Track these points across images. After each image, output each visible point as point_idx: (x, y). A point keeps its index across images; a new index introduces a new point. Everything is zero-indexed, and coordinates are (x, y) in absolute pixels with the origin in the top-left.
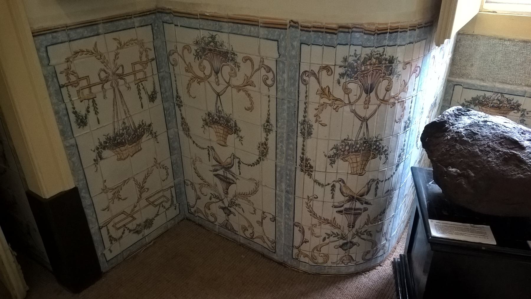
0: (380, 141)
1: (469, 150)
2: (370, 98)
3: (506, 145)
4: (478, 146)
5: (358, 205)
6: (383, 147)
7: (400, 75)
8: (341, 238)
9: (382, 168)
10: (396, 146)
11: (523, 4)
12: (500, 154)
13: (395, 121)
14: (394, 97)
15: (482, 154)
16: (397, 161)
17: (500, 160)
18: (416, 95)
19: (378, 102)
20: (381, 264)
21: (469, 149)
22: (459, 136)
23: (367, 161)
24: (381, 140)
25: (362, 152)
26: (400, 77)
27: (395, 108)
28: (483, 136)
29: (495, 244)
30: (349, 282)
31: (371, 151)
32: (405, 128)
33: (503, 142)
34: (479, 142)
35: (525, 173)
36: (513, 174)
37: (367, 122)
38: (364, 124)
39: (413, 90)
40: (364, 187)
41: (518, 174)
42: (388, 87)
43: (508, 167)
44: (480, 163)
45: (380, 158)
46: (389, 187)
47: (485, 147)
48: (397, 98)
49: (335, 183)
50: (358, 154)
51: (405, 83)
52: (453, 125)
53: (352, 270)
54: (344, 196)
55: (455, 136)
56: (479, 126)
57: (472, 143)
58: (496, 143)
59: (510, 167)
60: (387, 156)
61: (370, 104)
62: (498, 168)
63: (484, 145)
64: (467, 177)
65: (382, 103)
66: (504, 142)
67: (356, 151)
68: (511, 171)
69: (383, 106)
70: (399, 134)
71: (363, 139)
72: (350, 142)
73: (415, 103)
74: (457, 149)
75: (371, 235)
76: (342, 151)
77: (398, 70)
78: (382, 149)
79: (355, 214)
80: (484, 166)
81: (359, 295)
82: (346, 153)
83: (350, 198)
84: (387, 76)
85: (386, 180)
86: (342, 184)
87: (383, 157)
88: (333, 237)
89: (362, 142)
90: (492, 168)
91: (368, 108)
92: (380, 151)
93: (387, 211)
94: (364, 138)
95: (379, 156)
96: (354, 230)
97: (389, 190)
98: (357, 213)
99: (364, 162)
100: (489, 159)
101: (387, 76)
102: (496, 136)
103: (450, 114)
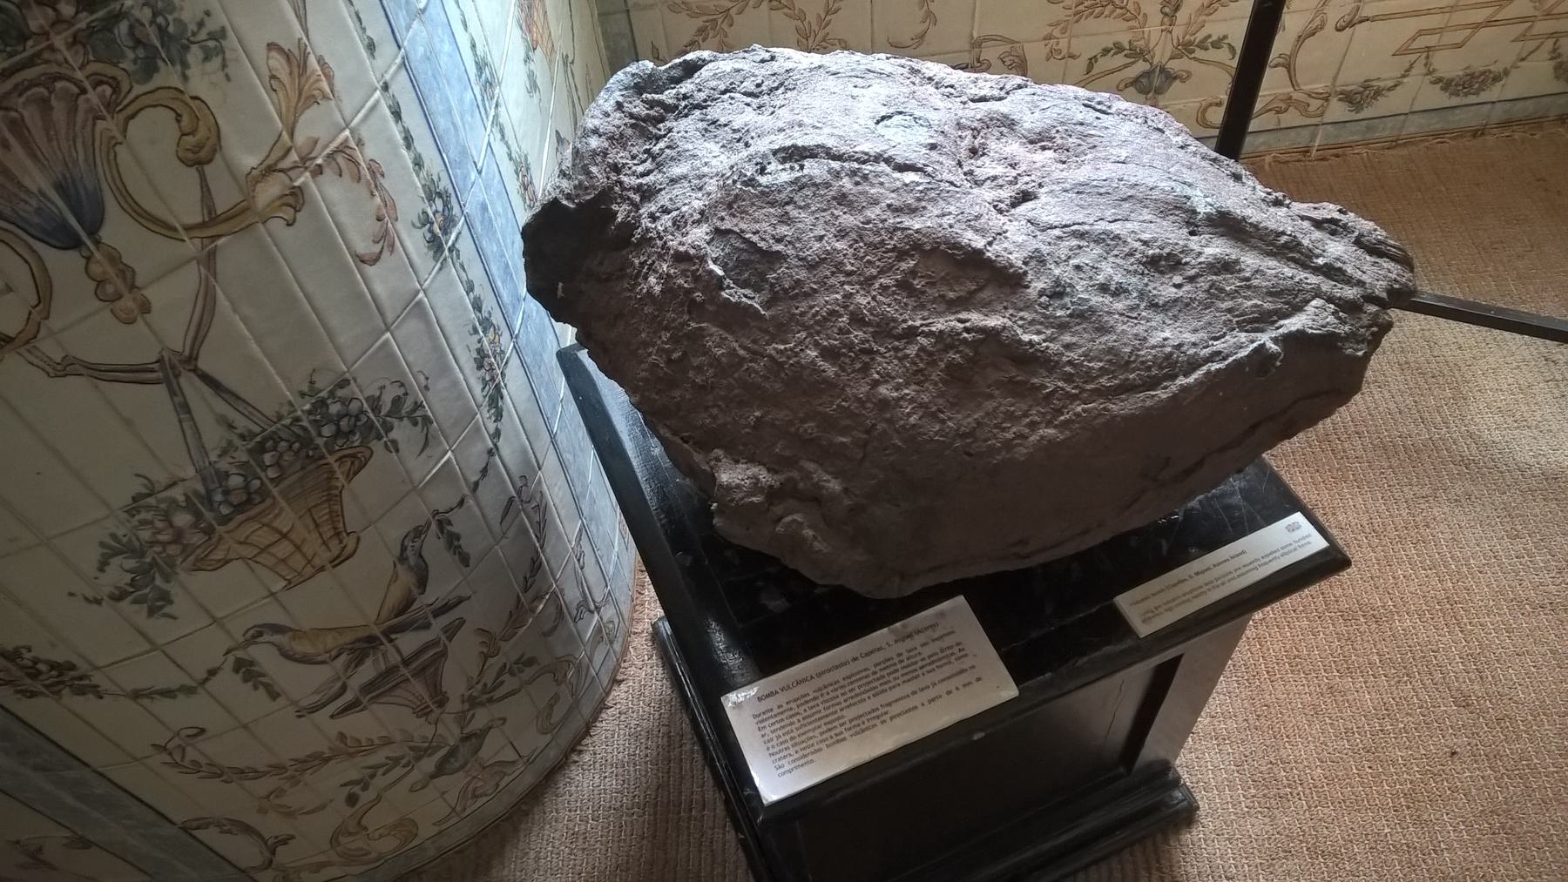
0: (340, 393)
1: (770, 356)
2: (114, 258)
3: (932, 284)
4: (806, 328)
5: (409, 642)
6: (375, 403)
7: (219, 35)
8: (418, 759)
9: (425, 469)
10: (437, 348)
11: (896, 701)
12: (922, 349)
13: (361, 260)
14: (271, 170)
15: (844, 370)
16: (477, 388)
17: (936, 384)
18: (405, 64)
19: (191, 247)
20: (618, 678)
21: (770, 350)
22: (697, 278)
23: (333, 497)
24: (344, 383)
25: (275, 491)
26: (231, 41)
27: (316, 215)
28: (812, 266)
29: (1010, 691)
30: (536, 829)
31: (323, 457)
32: (435, 245)
33: (913, 273)
34: (803, 307)
35: (1059, 412)
36: (1009, 435)
37: (195, 370)
38: (191, 387)
39: (364, 53)
40: (395, 578)
41: (1033, 426)
42: (189, 139)
43: (979, 406)
44: (847, 422)
45: (394, 446)
46: (505, 489)
47: (841, 331)
48: (294, 157)
49: (240, 654)
50: (262, 506)
51: (288, 56)
52: (648, 193)
53: (529, 780)
54: (323, 662)
55: (681, 281)
56: (772, 204)
57: (773, 317)
58: (884, 288)
59: (989, 405)
60: (418, 413)
61: (139, 282)
62: (937, 427)
63: (833, 314)
64: (815, 499)
65: (219, 236)
66: (922, 271)
67: (239, 508)
68: (996, 426)
69: (233, 253)
70: (421, 295)
71: (238, 442)
72: (177, 493)
73: (421, 102)
74: (717, 359)
75: (530, 662)
76: (164, 544)
77: (186, 16)
78: (376, 409)
79: (420, 673)
80: (868, 432)
81: (589, 869)
82: (196, 539)
83: (352, 650)
84: (138, 89)
85: (476, 484)
86: (277, 638)
87: (402, 432)
88: (384, 774)
89: (243, 457)
90: (911, 434)
91: (145, 308)
92: (370, 426)
93: (549, 554)
94: (242, 437)
95: (377, 446)
96: (454, 705)
97: (511, 500)
98: (428, 666)
99: (322, 514)
100: (883, 390)
101: (138, 89)
102: (875, 246)
103: (611, 138)
